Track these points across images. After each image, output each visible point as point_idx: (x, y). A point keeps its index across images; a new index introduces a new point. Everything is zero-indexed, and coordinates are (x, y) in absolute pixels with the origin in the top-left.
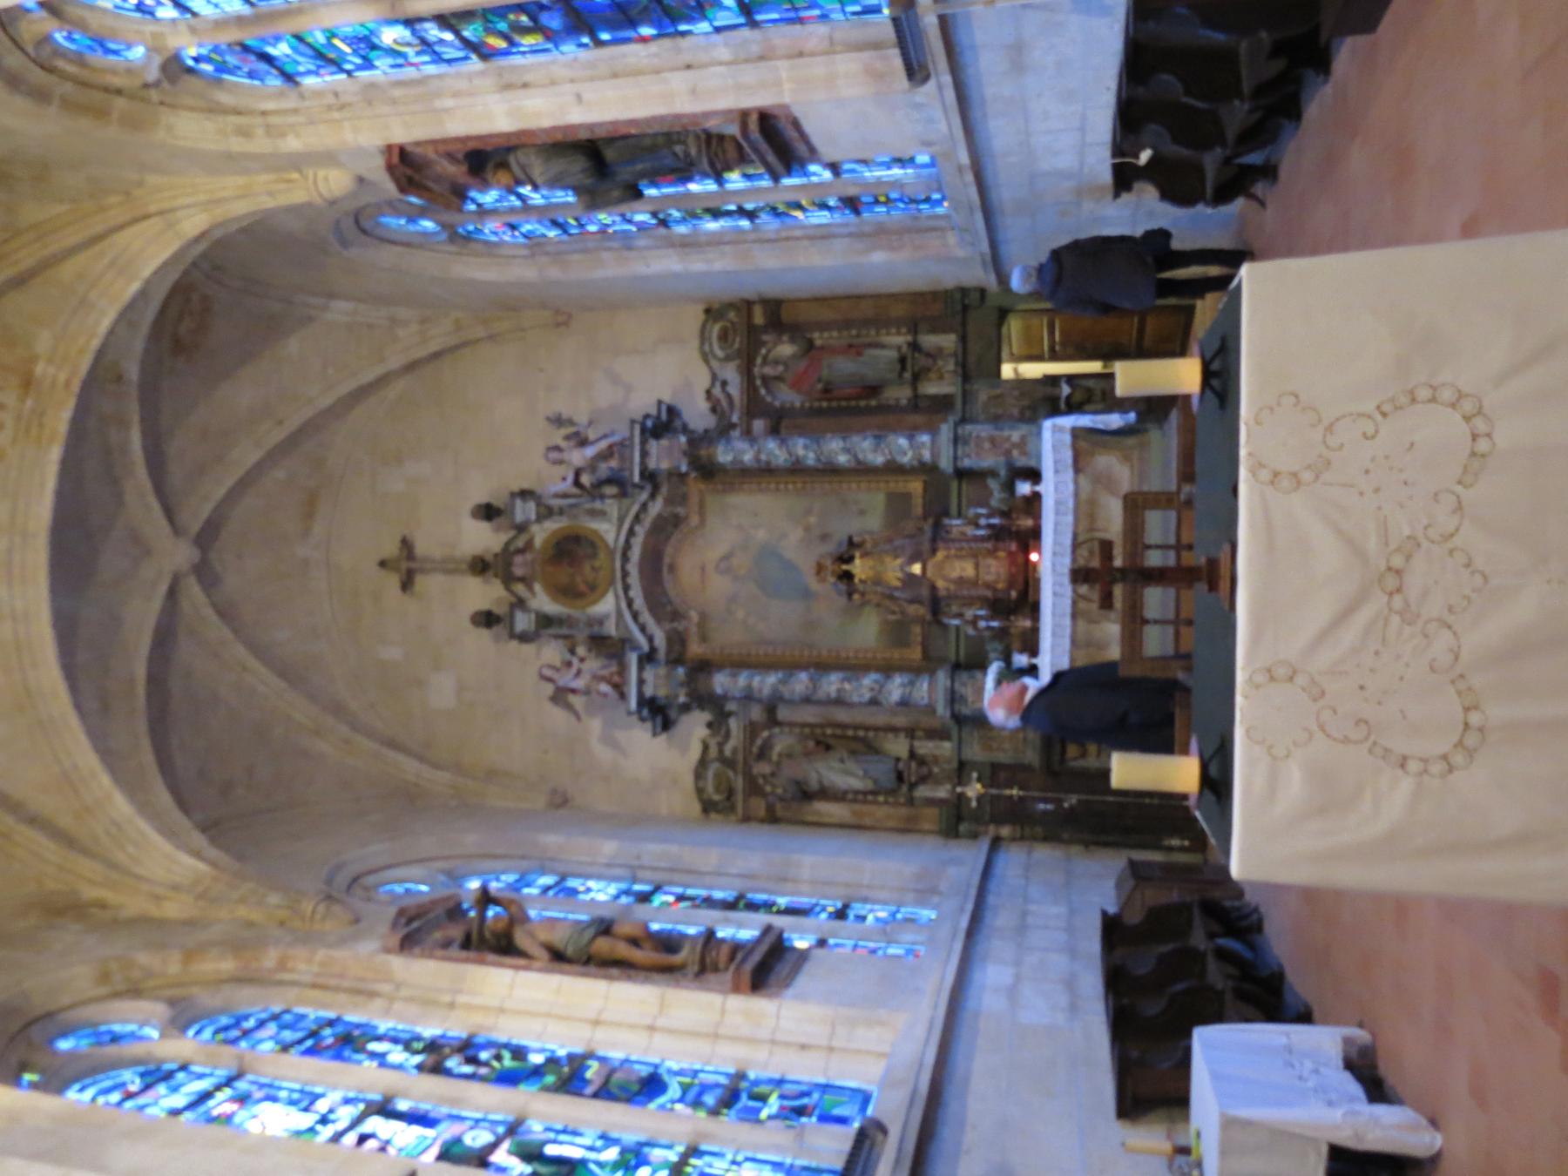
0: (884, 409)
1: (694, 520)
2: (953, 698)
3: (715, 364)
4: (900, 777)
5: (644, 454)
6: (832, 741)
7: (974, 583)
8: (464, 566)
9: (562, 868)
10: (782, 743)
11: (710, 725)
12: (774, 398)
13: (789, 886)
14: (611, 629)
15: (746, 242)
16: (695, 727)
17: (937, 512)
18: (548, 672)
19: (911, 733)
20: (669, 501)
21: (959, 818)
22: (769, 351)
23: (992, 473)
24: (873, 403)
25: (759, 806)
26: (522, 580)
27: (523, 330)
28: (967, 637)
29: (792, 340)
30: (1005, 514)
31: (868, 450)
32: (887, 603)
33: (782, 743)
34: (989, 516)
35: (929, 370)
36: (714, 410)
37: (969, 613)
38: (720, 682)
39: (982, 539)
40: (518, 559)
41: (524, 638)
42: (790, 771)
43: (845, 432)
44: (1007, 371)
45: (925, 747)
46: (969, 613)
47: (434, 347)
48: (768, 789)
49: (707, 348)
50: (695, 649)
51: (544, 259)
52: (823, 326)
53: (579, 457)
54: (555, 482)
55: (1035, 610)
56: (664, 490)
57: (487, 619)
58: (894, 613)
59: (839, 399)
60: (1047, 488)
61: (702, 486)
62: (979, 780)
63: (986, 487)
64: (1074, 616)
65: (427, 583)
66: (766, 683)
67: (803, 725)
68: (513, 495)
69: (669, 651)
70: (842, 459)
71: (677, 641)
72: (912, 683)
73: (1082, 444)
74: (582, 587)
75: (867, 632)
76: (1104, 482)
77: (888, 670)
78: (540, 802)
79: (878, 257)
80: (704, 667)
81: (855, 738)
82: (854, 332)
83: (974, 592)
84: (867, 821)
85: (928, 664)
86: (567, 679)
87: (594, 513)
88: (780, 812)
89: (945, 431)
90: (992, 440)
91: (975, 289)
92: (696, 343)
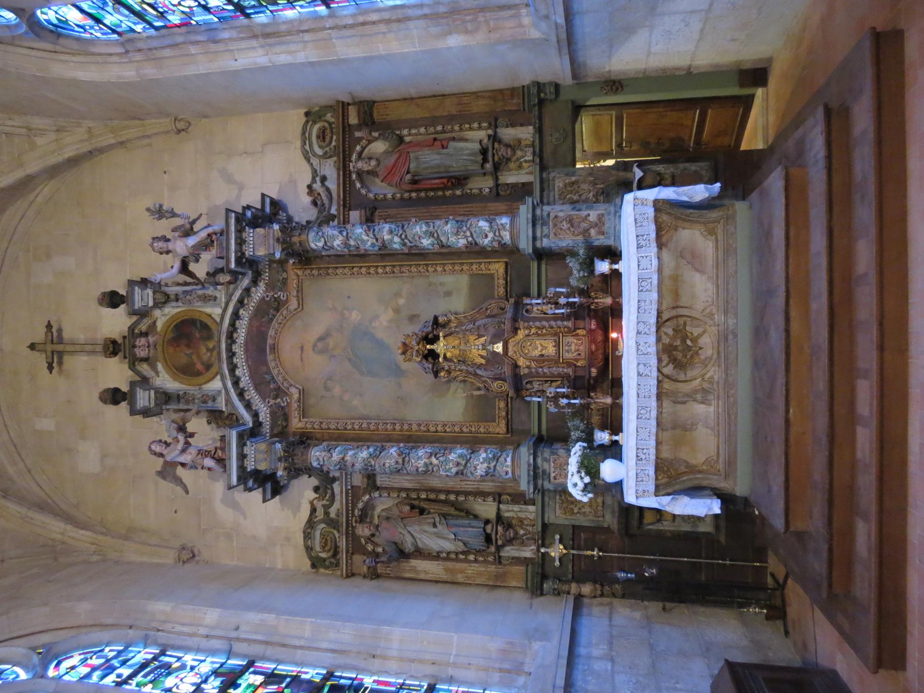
0: (468, 198)
1: (293, 304)
2: (536, 474)
3: (315, 161)
4: (488, 539)
5: (241, 242)
6: (424, 505)
7: (555, 361)
8: (99, 348)
9: (162, 637)
10: (383, 504)
11: (316, 489)
12: (369, 191)
13: (377, 664)
14: (221, 404)
15: (325, 29)
16: (304, 491)
17: (518, 293)
18: (157, 448)
19: (498, 497)
20: (270, 287)
21: (544, 577)
22: (363, 149)
23: (572, 253)
24: (458, 192)
25: (361, 563)
26: (146, 360)
27: (149, 137)
29: (382, 137)
30: (582, 293)
31: (451, 233)
32: (471, 379)
33: (383, 504)
34: (568, 296)
35: (509, 160)
36: (315, 203)
37: (551, 391)
38: (316, 455)
39: (563, 318)
40: (142, 341)
41: (146, 413)
42: (386, 535)
43: (429, 218)
44: (578, 166)
45: (511, 511)
46: (551, 391)
47: (69, 153)
48: (370, 547)
49: (307, 147)
50: (296, 423)
51: (139, 57)
52: (412, 124)
53: (182, 246)
54: (165, 270)
55: (616, 387)
56: (266, 276)
57: (114, 396)
58: (479, 389)
59: (427, 190)
60: (628, 267)
61: (299, 272)
62: (561, 542)
63: (567, 265)
64: (659, 397)
65: (76, 363)
66: (360, 456)
67: (400, 490)
68: (131, 283)
69: (272, 429)
70: (426, 242)
71: (281, 415)
72: (496, 458)
73: (665, 218)
74: (199, 367)
75: (452, 407)
76: (691, 258)
77: (474, 443)
78: (169, 557)
79: (455, 41)
80: (305, 440)
81: (446, 502)
82: (439, 128)
83: (555, 370)
84: (460, 578)
85: (513, 437)
86: (172, 454)
87: (206, 299)
88: (380, 569)
89: (524, 211)
90: (571, 221)
91: (550, 83)
92: (298, 143)
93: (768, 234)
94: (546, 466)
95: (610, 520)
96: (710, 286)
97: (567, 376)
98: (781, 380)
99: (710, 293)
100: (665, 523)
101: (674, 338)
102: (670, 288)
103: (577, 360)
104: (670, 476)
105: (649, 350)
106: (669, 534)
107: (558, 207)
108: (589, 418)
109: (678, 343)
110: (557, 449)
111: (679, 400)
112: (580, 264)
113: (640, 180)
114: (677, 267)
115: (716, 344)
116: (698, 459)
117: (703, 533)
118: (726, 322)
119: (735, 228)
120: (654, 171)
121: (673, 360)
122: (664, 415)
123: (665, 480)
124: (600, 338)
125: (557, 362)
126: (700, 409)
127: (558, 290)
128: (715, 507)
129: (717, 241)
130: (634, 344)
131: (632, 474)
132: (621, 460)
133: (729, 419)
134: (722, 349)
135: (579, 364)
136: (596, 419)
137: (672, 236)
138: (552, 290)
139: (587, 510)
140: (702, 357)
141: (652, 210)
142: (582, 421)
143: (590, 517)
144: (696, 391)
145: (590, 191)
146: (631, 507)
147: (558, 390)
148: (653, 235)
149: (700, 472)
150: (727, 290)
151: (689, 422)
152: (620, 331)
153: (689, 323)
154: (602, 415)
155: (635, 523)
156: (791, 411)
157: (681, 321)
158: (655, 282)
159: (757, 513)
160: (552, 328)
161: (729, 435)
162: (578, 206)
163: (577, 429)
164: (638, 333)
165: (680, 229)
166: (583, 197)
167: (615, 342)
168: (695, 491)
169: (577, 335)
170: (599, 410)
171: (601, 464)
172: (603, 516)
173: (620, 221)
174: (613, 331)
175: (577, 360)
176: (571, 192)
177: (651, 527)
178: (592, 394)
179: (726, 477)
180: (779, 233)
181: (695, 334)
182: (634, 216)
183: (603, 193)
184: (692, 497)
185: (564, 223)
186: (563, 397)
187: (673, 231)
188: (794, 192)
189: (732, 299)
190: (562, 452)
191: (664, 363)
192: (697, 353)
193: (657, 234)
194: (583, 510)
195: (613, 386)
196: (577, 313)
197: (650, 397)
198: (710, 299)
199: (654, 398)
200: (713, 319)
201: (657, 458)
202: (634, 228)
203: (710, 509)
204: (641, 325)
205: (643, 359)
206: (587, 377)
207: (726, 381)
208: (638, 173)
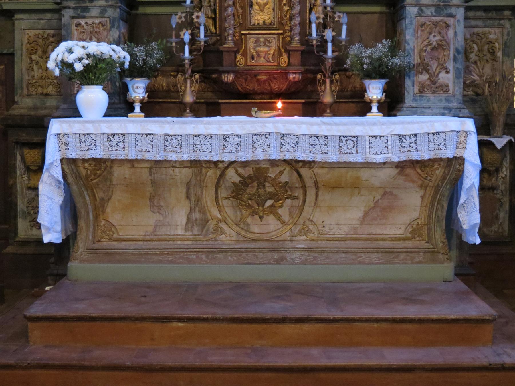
7: (244, 24)
23: (395, 48)
28: (170, 15)
30: (339, 64)
37: (201, 18)
39: (305, 34)
46: (201, 18)
55: (209, 108)
60: (375, 123)
63: (378, 40)
64: (195, 163)
76: (384, 204)
83: (230, 22)
90: (440, 47)
93: (410, 300)
94: (94, 12)
95: (24, 105)
96: (346, 229)
97: (221, 37)
98: (220, 312)
99: (335, 230)
100: (26, 177)
101: (274, 182)
102: (342, 178)
103: (244, 54)
104: (88, 178)
105: (260, 150)
106: (11, 182)
107: (460, 28)
108: (164, 73)
109: (269, 189)
110: (119, 27)
111: (192, 191)
112: (380, 59)
113: (491, 144)
114: (371, 188)
115: (264, 237)
116: (114, 216)
117: (16, 225)
118: (296, 250)
119: (420, 262)
120: (501, 163)
121: (245, 182)
122: (170, 171)
123: (84, 172)
124: (275, 86)
125: (242, 26)
126: (180, 217)
127: (345, 28)
128: (52, 235)
129: (404, 240)
130: (269, 131)
131: (90, 129)
132: (105, 116)
133: (168, 254)
134: (259, 245)
135: (239, 57)
136: (162, 82)
137: (413, 182)
138: (344, 19)
139: (37, 73)
140: (249, 220)
141: (450, 155)
142: (160, 61)
143: (26, 77)
144: (203, 211)
145: (481, 76)
146: (45, 128)
147: (202, 28)
148: (415, 156)
149: (96, 218)
150: (338, 252)
151: (162, 203)
152: (287, 112)
153: (296, 203)
154: (168, 91)
155: (24, 137)
156: (180, 324)
157: (298, 193)
158: (352, 159)
159: (47, 288)
160: (291, 19)
161: (147, 254)
162: (461, 57)
163: (148, 54)
164: (283, 136)
165: (422, 193)
166: (473, 67)
167: (270, 107)
168: (71, 211)
169: (280, 55)
170: (175, 86)
171: (101, 87)
172: (29, 95)
173: (437, 114)
174: (283, 103)
175: (244, 54)
176: (480, 50)
177: (19, 158)
178: (197, 76)
179: (92, 251)
180: (411, 311)
181: (280, 211)
182: (445, 131)
183: (477, 95)
184: (63, 207)
185: (438, 38)
186: (192, 34)
187: (420, 182)
188: (462, 329)
189: (327, 258)
190: (115, 34)
191: (240, 170)
192: (255, 213)
193: (417, 162)
194: (35, 68)
195: (208, 104)
196: (311, 55)
197: (195, 151)
198: (326, 229)
199: (193, 157)
200: (300, 233)
201: (112, 161)
202: (426, 130)
203: (49, 230)
204: (294, 140)
205: (247, 142)
206: (221, 69)
207: (220, 250)
208: (500, 142)
